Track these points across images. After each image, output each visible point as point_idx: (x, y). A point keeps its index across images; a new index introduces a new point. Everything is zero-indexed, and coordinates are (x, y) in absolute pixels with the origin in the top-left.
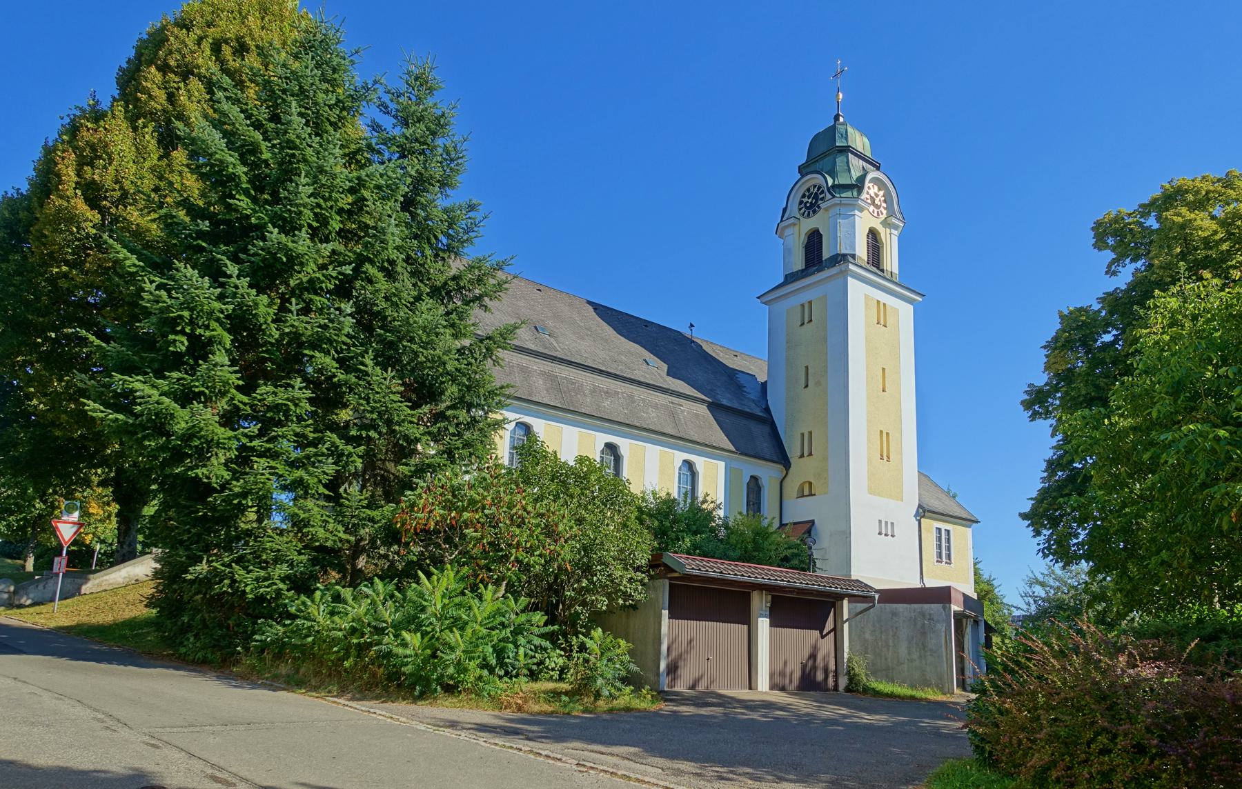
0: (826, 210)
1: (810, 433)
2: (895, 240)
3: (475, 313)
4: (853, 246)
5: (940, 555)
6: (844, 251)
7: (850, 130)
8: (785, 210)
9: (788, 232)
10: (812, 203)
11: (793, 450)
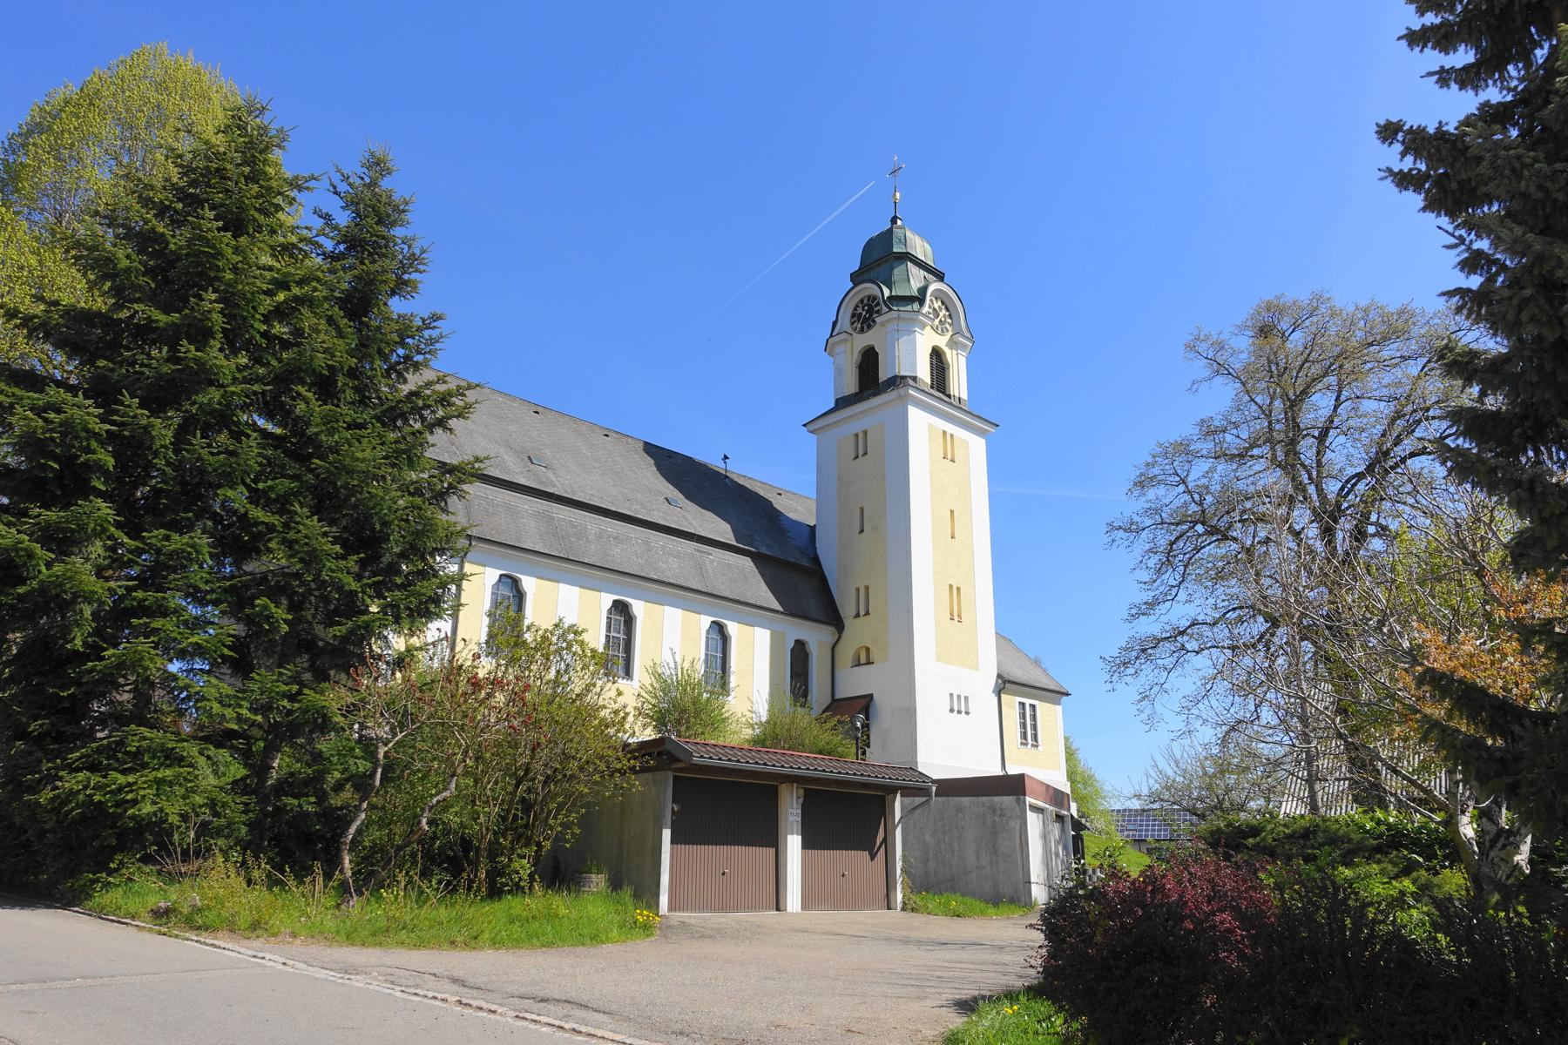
0: (883, 324)
1: (867, 588)
2: (963, 361)
3: (439, 436)
4: (914, 368)
5: (1024, 736)
6: (903, 373)
7: (909, 234)
8: (835, 324)
9: (839, 349)
10: (866, 314)
11: (847, 611)
